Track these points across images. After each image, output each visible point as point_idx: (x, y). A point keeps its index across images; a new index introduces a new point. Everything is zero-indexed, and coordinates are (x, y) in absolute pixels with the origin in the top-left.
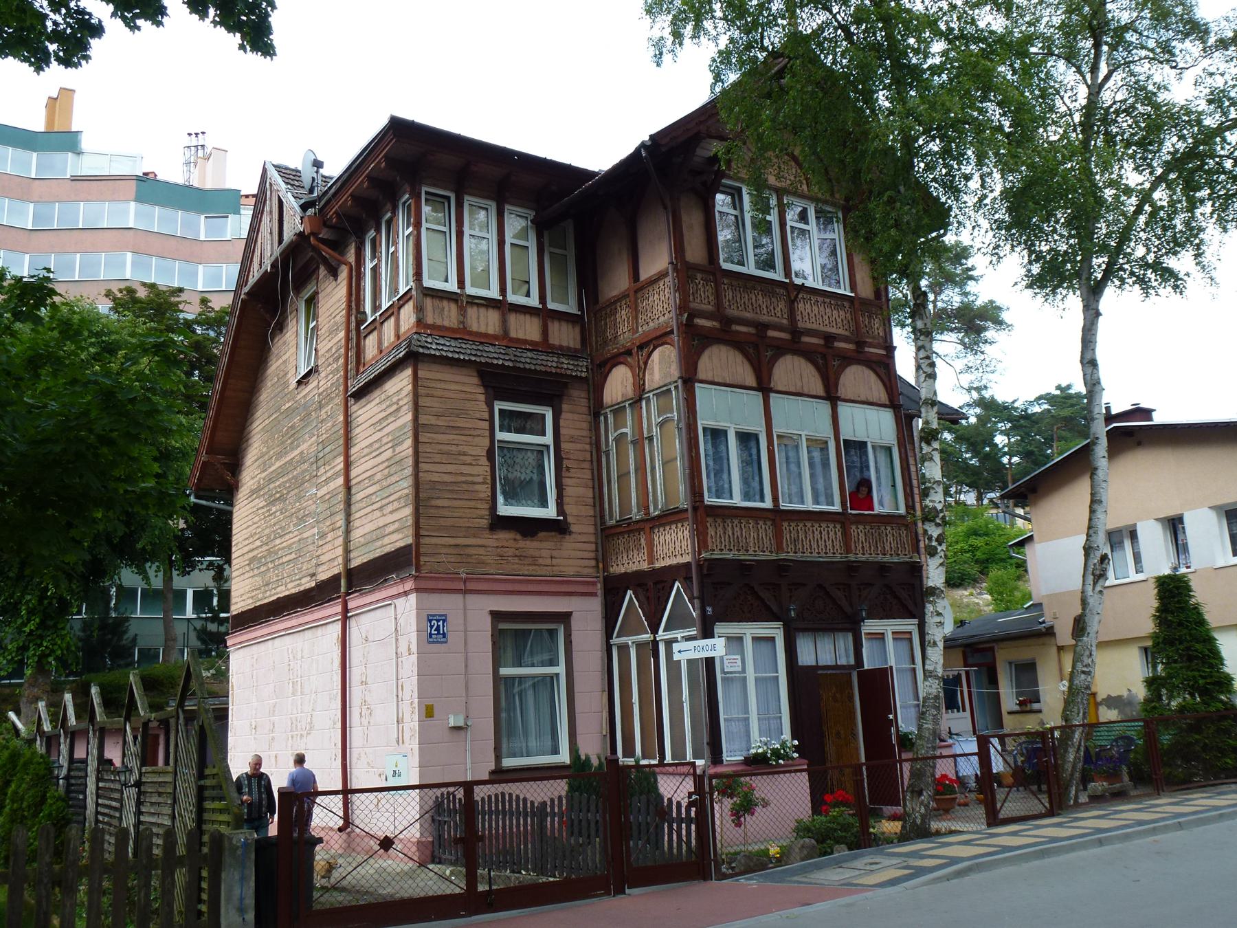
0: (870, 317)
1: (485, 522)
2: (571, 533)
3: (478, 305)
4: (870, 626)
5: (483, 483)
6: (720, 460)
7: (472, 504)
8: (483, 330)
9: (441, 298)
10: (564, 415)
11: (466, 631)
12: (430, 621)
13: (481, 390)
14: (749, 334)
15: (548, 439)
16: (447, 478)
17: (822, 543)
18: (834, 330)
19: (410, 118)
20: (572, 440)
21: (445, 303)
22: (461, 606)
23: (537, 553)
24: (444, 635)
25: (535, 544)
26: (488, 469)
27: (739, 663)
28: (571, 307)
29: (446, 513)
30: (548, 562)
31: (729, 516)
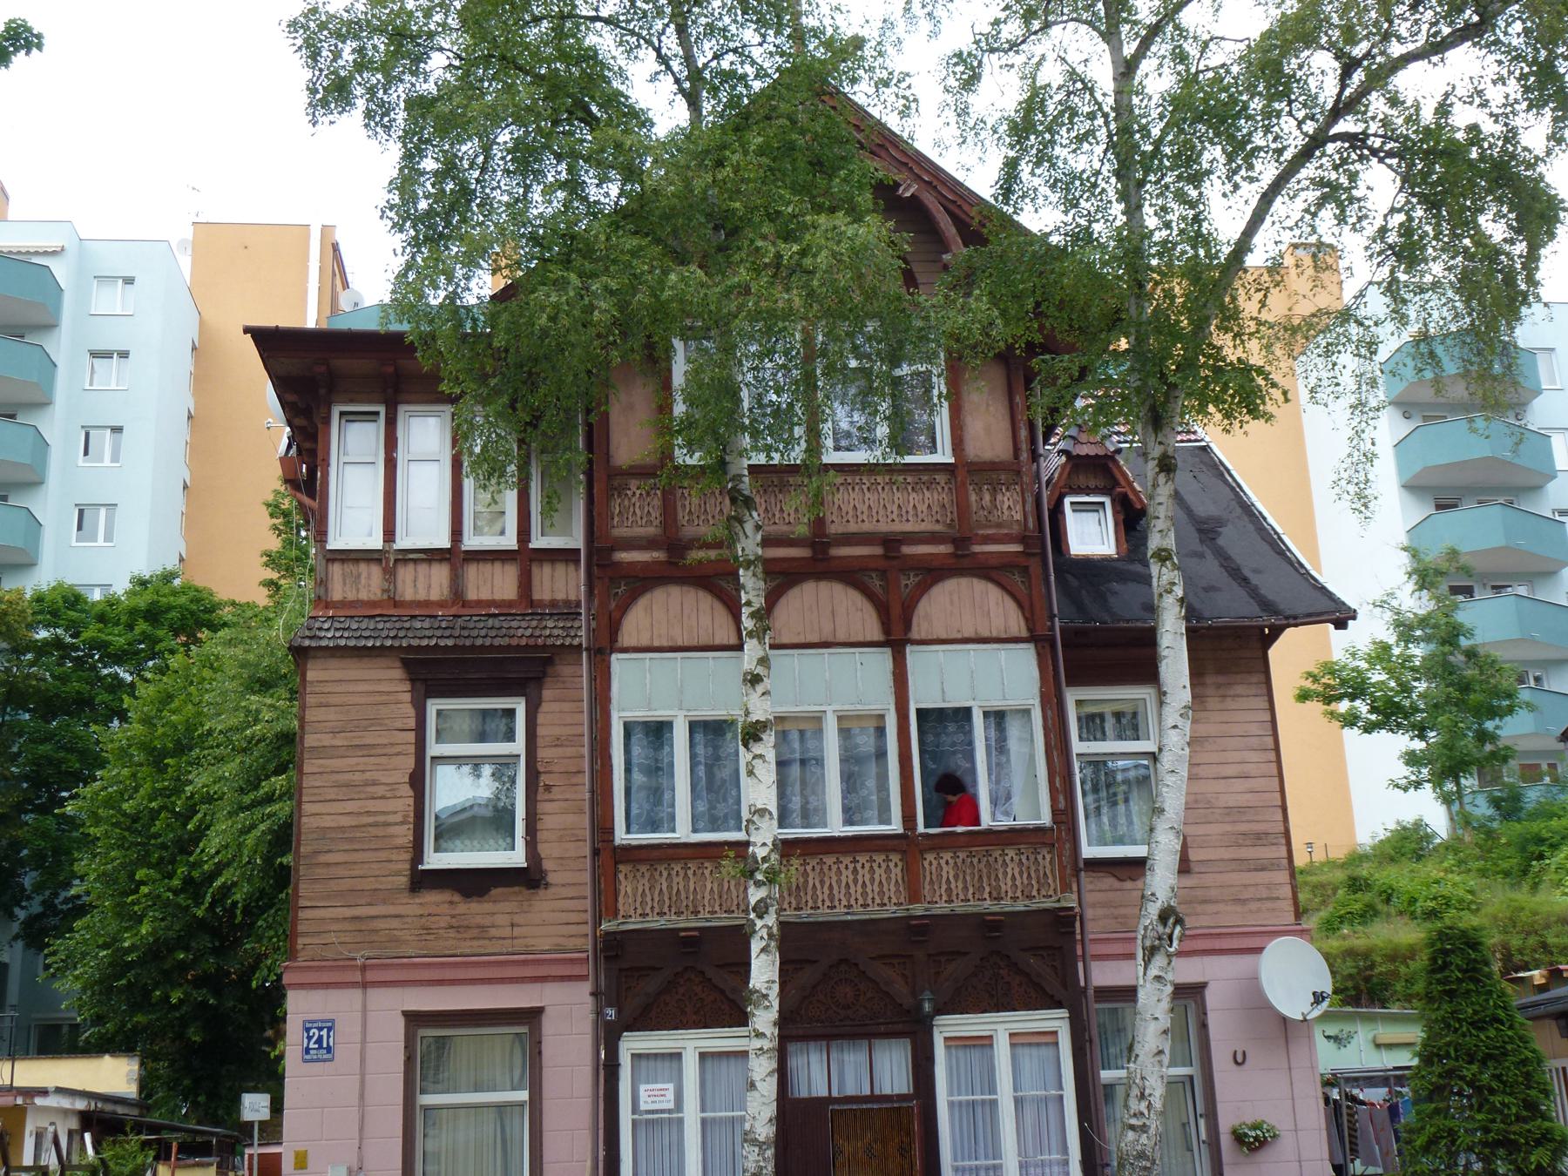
0: (994, 492)
1: (403, 881)
2: (547, 885)
3: (415, 561)
4: (948, 1026)
5: (402, 823)
6: (659, 770)
7: (383, 855)
8: (422, 596)
9: (357, 561)
10: (545, 707)
11: (364, 1041)
12: (308, 1030)
13: (407, 686)
14: (655, 562)
15: (519, 746)
16: (346, 821)
17: (856, 891)
18: (899, 527)
19: (273, 324)
20: (558, 742)
21: (363, 567)
22: (358, 1006)
23: (487, 921)
24: (329, 1049)
25: (487, 907)
26: (411, 802)
27: (671, 1095)
28: (575, 539)
29: (340, 872)
30: (507, 932)
31: (660, 860)
